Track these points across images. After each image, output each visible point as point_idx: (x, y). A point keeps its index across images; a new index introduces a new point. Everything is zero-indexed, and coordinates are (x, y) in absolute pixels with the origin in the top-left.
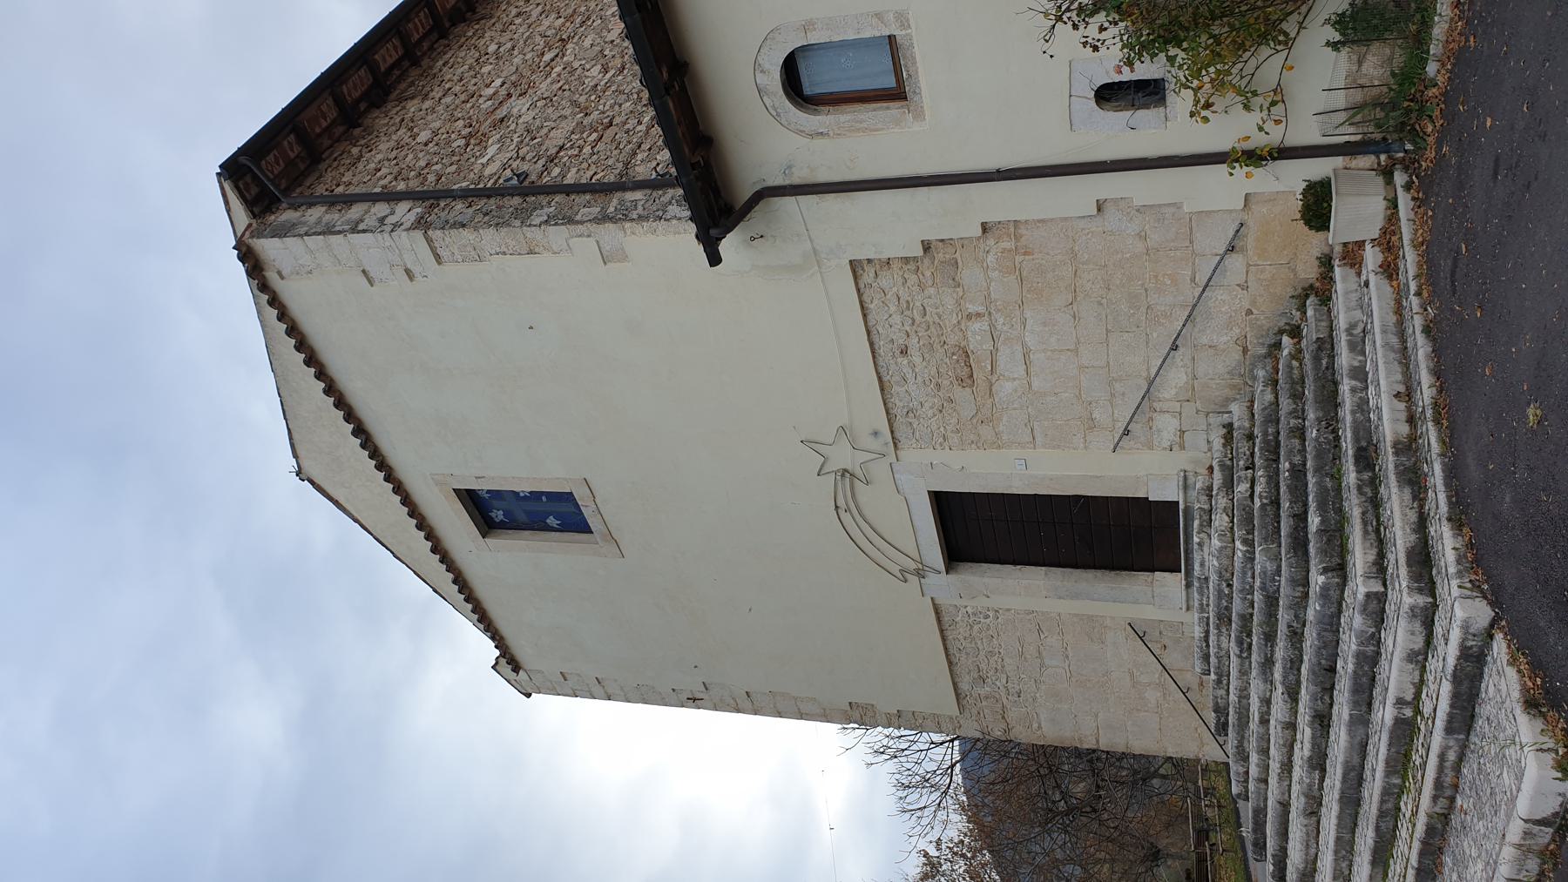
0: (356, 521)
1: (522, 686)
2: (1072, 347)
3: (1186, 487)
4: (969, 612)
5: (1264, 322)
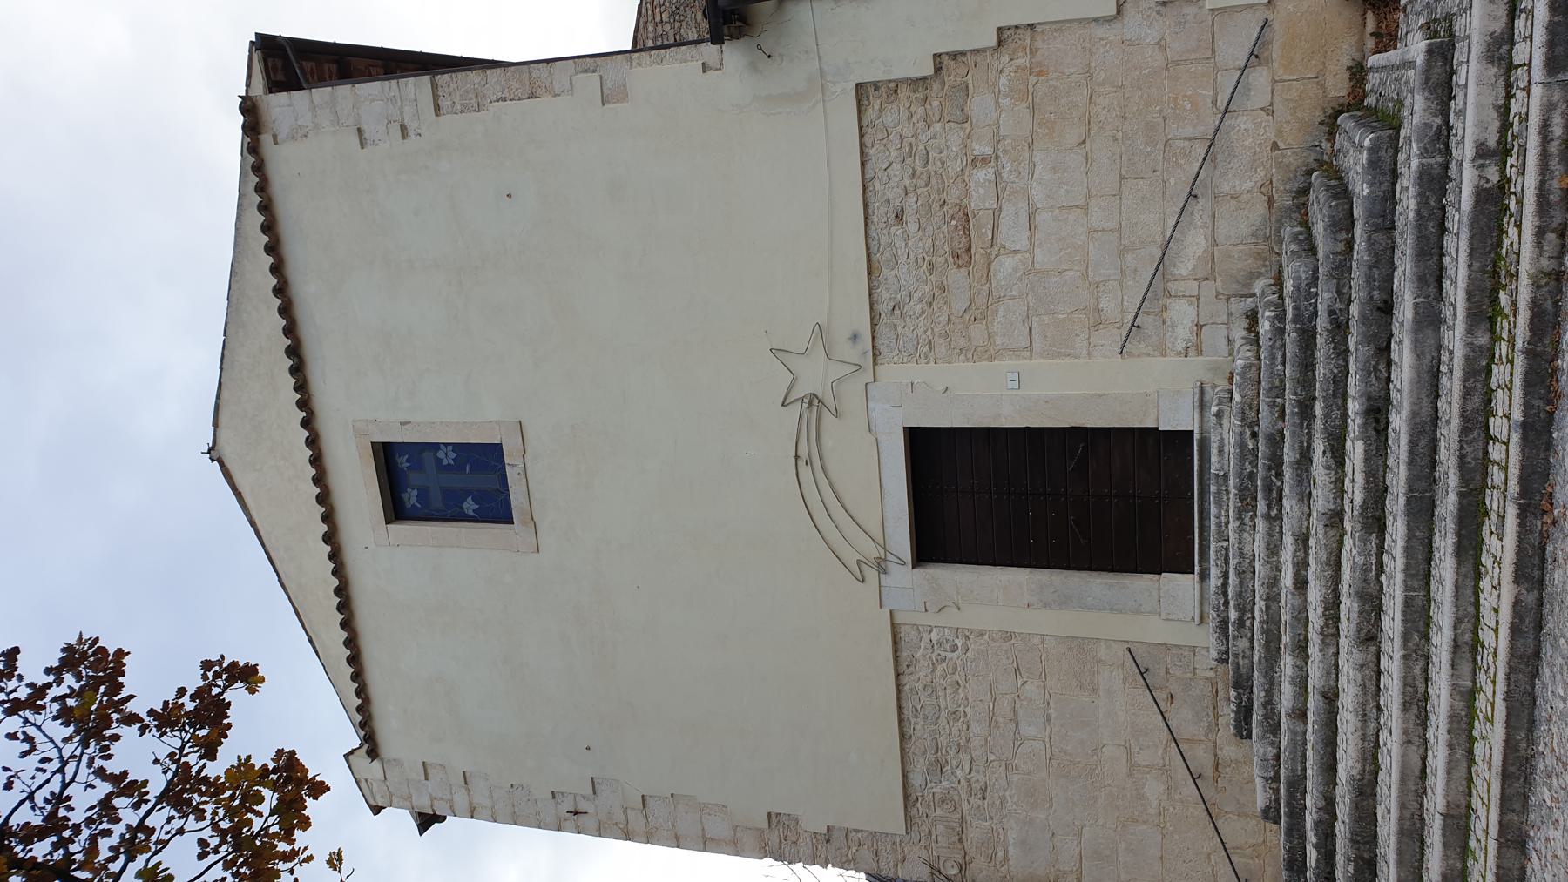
0: (253, 524)
1: (371, 791)
2: (1081, 202)
3: (1203, 406)
4: (934, 642)
5: (1291, 159)
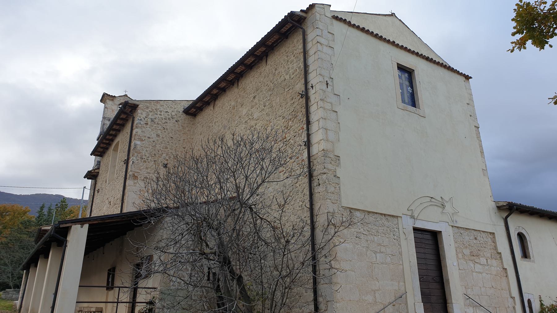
0: (379, 15)
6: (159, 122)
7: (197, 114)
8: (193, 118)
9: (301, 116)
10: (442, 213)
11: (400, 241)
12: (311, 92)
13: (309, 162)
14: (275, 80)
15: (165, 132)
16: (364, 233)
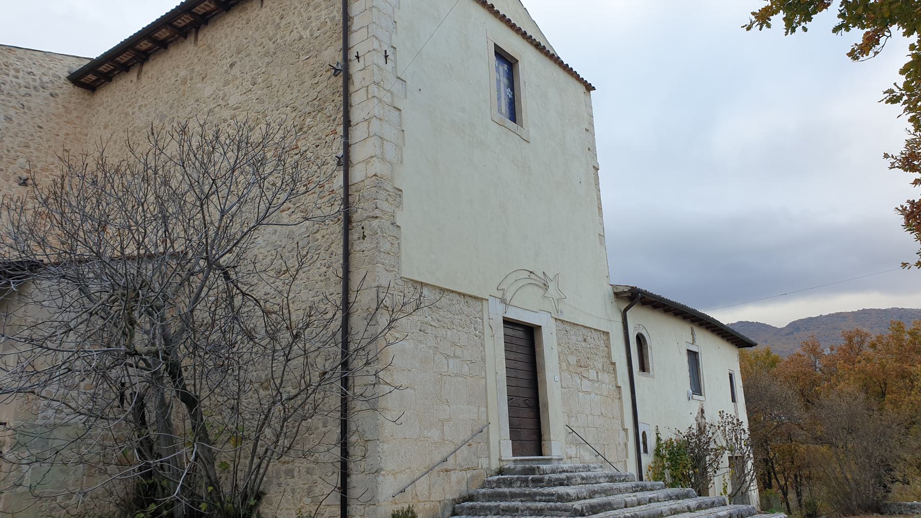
6: (11, 92)
7: (98, 86)
8: (89, 94)
9: (333, 108)
10: (544, 297)
11: (483, 340)
12: (355, 68)
13: (347, 195)
14: (278, 36)
15: (25, 113)
16: (433, 323)
